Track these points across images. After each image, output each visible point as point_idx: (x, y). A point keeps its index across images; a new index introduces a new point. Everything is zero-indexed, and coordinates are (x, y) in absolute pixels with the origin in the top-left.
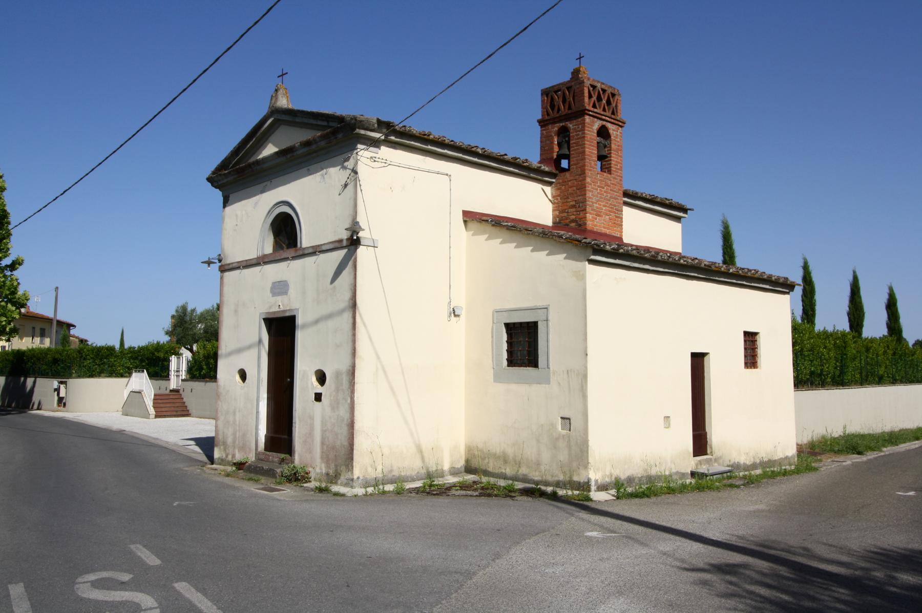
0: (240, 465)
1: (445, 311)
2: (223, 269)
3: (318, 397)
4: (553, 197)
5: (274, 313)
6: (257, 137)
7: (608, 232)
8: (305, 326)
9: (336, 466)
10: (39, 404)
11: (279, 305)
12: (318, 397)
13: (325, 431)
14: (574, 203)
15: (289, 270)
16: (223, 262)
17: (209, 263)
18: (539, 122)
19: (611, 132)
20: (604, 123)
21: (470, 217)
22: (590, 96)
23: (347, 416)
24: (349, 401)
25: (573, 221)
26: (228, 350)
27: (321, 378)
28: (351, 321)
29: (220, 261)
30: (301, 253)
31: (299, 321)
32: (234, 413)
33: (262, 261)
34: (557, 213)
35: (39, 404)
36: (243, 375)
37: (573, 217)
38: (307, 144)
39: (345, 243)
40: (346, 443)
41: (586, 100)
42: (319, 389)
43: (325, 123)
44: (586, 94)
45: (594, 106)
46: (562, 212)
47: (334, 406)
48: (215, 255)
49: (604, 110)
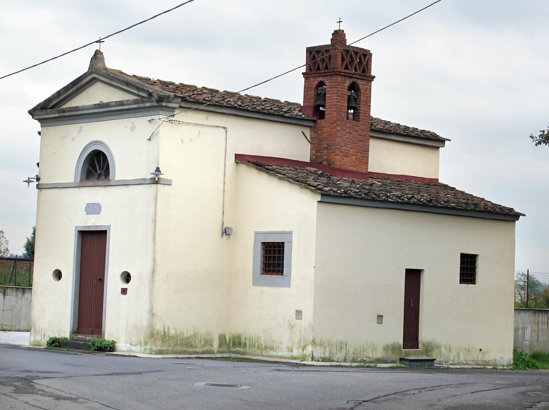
1: (219, 231)
3: (124, 291)
4: (311, 138)
6: (78, 86)
7: (354, 169)
11: (93, 222)
12: (124, 291)
14: (325, 146)
15: (95, 194)
16: (41, 182)
17: (29, 181)
18: (313, 54)
19: (361, 86)
20: (355, 80)
21: (240, 159)
22: (343, 59)
25: (326, 160)
27: (127, 277)
29: (38, 179)
34: (314, 152)
36: (58, 275)
37: (325, 157)
38: (121, 103)
41: (340, 63)
42: (125, 286)
44: (340, 59)
45: (346, 68)
46: (317, 152)
48: (34, 176)
49: (356, 70)
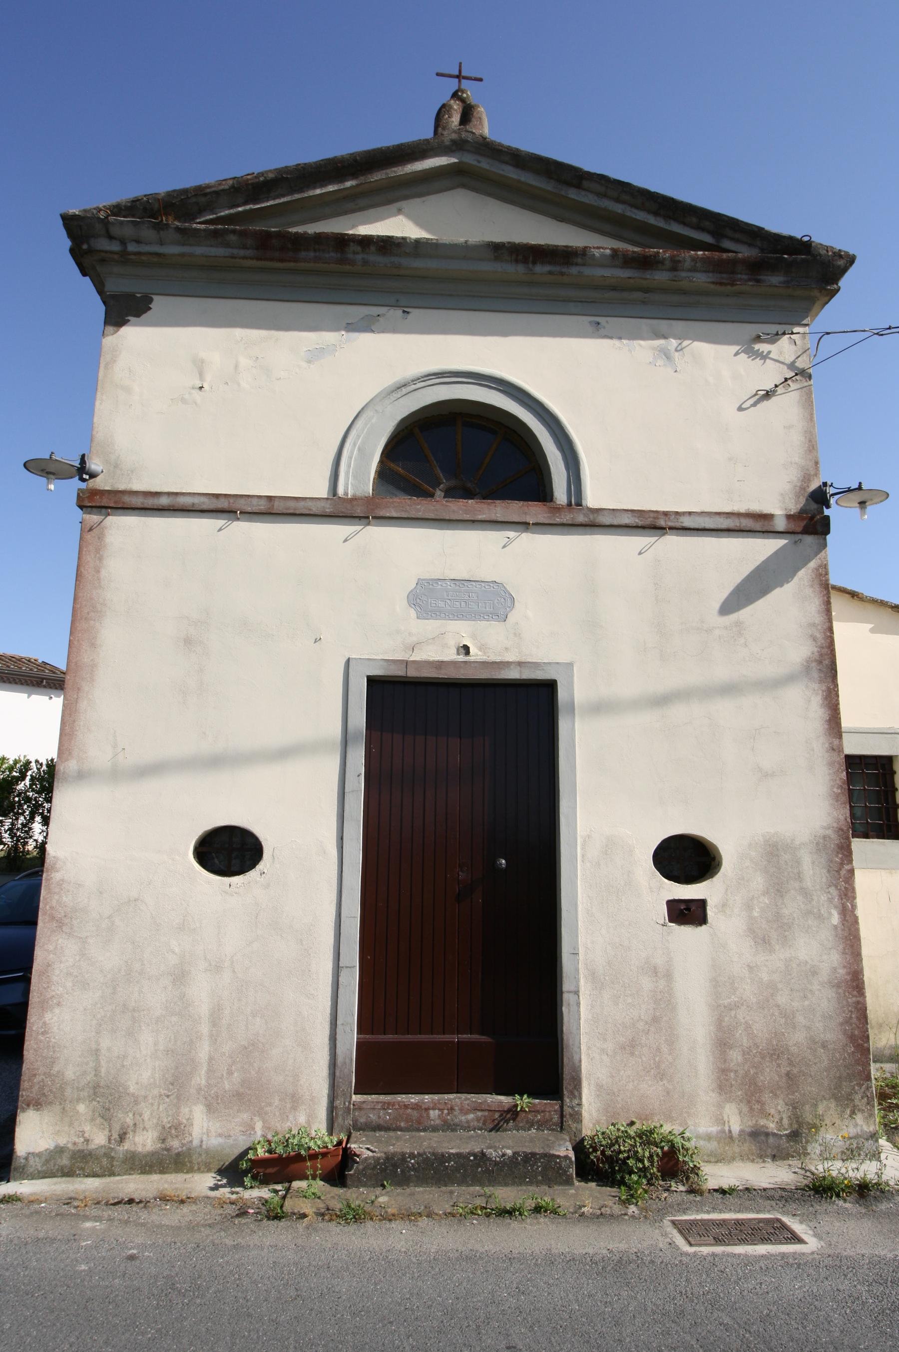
0: (278, 1166)
2: (100, 503)
5: (440, 664)
8: (600, 708)
9: (794, 1106)
10: (408, 313)
13: (729, 1008)
23: (831, 960)
24: (835, 919)
26: (840, 629)
27: (686, 858)
28: (817, 712)
30: (581, 519)
31: (576, 692)
32: (180, 976)
33: (338, 510)
35: (408, 313)
39: (781, 524)
40: (833, 1035)
43: (707, 238)
47: (769, 933)
